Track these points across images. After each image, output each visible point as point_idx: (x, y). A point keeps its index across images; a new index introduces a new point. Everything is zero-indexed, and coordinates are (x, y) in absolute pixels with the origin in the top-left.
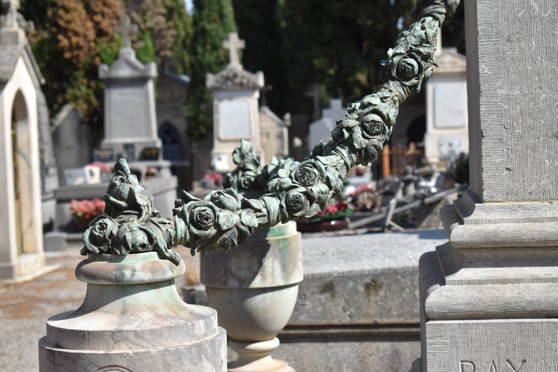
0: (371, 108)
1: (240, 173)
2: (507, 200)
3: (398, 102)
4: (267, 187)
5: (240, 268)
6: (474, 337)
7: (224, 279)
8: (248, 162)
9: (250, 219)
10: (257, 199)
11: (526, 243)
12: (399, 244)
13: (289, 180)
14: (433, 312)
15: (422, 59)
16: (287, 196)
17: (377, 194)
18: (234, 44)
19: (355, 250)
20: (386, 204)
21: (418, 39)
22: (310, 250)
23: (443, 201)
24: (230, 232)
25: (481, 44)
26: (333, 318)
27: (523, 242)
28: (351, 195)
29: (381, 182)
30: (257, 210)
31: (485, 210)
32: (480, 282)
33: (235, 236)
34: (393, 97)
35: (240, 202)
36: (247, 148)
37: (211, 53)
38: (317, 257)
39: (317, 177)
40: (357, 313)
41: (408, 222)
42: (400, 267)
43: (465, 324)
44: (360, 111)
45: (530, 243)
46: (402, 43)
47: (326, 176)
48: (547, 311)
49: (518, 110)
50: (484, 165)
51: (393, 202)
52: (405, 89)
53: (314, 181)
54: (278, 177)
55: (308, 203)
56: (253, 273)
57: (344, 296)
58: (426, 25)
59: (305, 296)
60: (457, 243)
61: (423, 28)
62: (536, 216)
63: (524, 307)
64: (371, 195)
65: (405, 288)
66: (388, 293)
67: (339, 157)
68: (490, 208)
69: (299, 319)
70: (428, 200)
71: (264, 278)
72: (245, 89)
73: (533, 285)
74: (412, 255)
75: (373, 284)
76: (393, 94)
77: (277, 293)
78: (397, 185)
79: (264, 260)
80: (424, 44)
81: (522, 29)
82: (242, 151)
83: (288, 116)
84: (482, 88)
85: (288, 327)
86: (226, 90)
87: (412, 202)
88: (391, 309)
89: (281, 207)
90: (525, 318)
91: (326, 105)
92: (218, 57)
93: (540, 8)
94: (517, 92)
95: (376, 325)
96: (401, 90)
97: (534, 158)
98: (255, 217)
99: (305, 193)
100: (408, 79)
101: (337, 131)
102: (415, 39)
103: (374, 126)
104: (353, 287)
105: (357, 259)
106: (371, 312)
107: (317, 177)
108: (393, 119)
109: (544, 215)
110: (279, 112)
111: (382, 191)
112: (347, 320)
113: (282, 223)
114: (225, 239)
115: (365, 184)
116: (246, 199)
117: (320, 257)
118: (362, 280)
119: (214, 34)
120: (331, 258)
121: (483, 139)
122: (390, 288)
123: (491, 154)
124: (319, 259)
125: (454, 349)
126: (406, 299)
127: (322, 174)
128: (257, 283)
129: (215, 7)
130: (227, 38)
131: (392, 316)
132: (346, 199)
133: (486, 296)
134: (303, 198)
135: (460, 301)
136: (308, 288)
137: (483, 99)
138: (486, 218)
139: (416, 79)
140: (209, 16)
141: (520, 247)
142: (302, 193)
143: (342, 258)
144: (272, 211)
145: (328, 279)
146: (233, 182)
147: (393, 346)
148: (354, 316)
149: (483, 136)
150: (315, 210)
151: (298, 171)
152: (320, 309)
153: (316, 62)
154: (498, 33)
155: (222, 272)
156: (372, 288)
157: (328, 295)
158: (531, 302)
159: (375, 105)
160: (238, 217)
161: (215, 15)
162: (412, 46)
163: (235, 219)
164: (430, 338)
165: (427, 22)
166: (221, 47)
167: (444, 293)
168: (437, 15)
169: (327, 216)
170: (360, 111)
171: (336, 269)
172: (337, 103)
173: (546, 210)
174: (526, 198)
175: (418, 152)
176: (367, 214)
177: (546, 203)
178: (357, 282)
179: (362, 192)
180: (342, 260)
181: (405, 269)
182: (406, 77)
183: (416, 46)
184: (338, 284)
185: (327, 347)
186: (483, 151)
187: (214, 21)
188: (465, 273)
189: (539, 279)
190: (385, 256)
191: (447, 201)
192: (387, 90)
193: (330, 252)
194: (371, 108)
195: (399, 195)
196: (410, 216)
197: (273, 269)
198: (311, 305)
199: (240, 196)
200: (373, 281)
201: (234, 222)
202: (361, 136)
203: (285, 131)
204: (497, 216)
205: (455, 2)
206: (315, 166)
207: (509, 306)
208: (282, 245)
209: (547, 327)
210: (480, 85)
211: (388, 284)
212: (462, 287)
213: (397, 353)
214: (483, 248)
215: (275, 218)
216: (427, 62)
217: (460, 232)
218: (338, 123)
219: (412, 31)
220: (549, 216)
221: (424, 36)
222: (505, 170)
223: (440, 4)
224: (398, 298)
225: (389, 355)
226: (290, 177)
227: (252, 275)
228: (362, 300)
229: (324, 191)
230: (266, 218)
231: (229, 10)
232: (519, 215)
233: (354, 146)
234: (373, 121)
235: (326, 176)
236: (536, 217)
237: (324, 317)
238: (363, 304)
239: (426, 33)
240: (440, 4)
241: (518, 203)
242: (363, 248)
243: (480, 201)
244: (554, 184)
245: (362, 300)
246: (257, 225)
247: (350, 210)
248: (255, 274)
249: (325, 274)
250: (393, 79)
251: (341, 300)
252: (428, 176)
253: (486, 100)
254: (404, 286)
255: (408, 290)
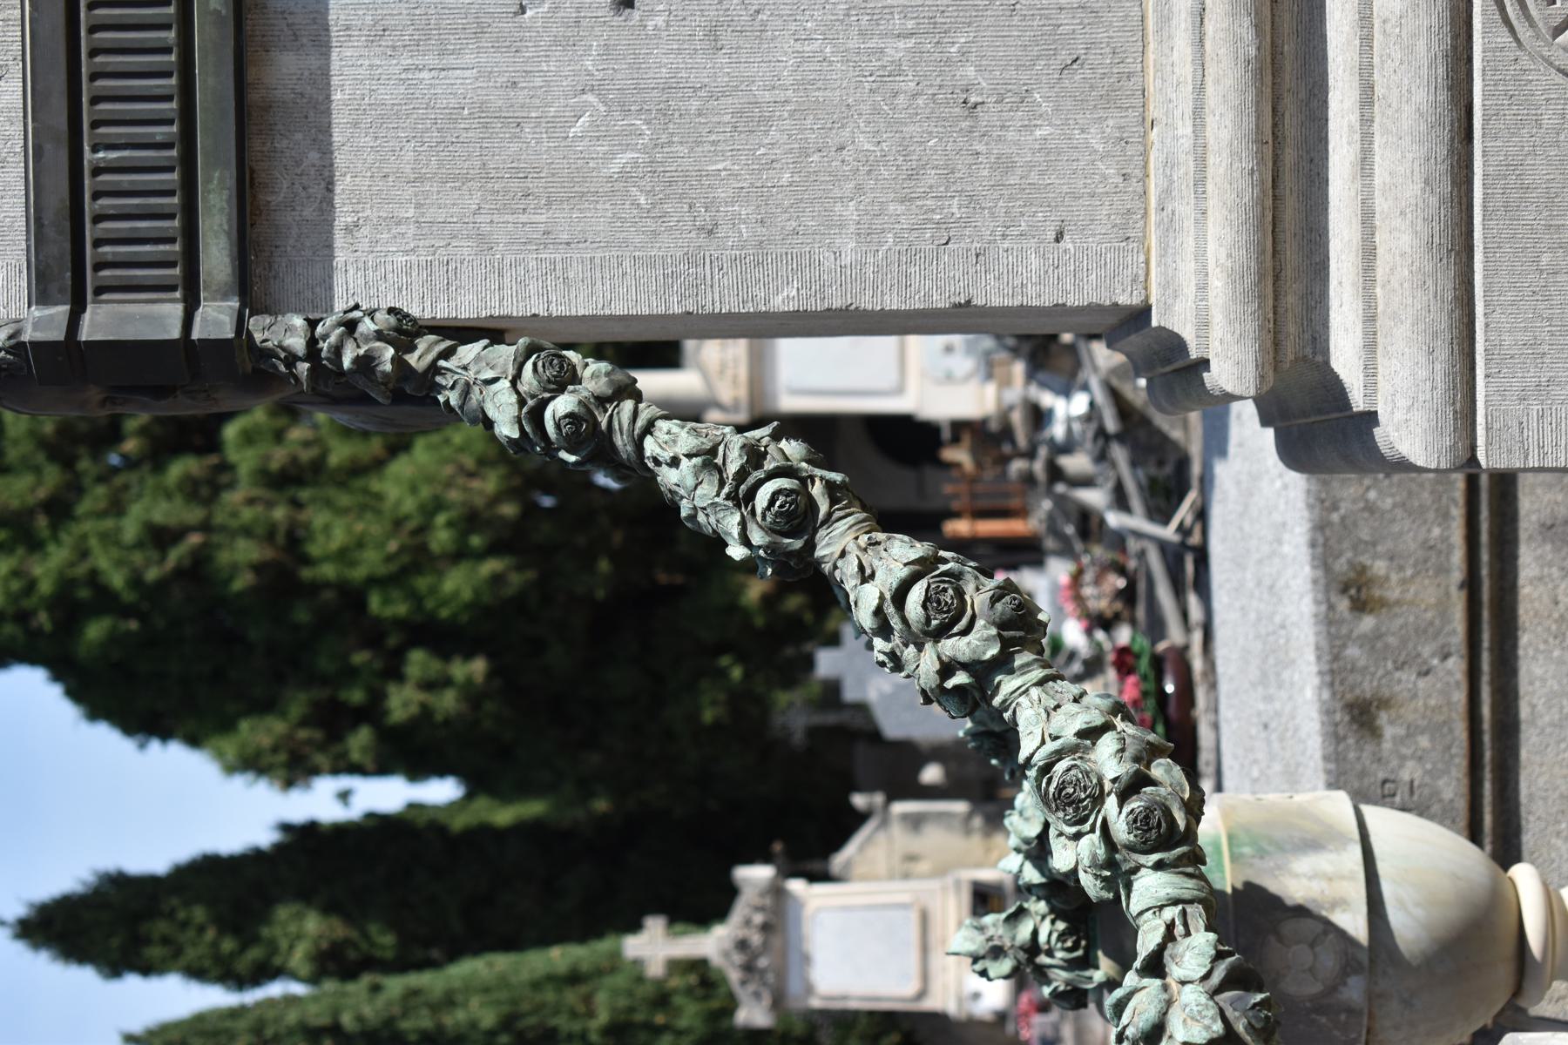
0: (890, 609)
1: (1043, 959)
2: (1143, 240)
3: (873, 535)
4: (1102, 903)
5: (1311, 970)
6: (1522, 337)
7: (1343, 1017)
8: (1013, 938)
9: (1195, 953)
10: (1136, 933)
11: (1263, 191)
12: (1242, 515)
13: (1085, 840)
14: (1453, 447)
15: (759, 466)
16: (1131, 848)
17: (1085, 560)
18: (653, 946)
19: (1258, 637)
20: (1118, 540)
21: (704, 476)
22: (1255, 761)
23: (1115, 382)
24: (1230, 1013)
25: (717, 304)
26: (1449, 703)
27: (1260, 202)
28: (1089, 632)
29: (1050, 543)
30: (1169, 936)
31: (1170, 301)
32: (1370, 319)
33: (1239, 998)
34: (859, 547)
35: (1146, 981)
36: (972, 940)
37: (678, 1012)
38: (1276, 745)
39: (1078, 762)
40: (1436, 636)
41: (1170, 481)
42: (1306, 514)
43: (1488, 361)
44: (897, 639)
45: (1262, 182)
46: (712, 520)
47: (1074, 740)
48: (1452, 139)
49: (901, 208)
50: (1047, 300)
51: (1114, 519)
52: (838, 514)
53: (1087, 773)
54: (1074, 871)
55: (1148, 789)
56: (1325, 933)
57: (1388, 673)
58: (666, 455)
59: (1385, 782)
60: (1262, 377)
61: (674, 462)
62: (1188, 166)
63: (1442, 201)
64: (1088, 577)
65: (1367, 501)
66: (1379, 548)
67: (1021, 699)
68: (1165, 286)
69: (1452, 801)
70: (1111, 425)
71: (1340, 903)
72: (778, 918)
73: (1380, 177)
74: (1272, 481)
75: (1353, 592)
76: (851, 547)
77: (1382, 867)
78: (1061, 501)
79: (1289, 902)
80: (719, 460)
81: (682, 197)
82: (982, 952)
83: (859, 800)
84: (837, 303)
85: (1475, 836)
86: (781, 973)
87: (1114, 465)
88: (1425, 541)
89: (1159, 866)
90: (1472, 198)
91: (833, 688)
92: (689, 991)
93: (628, 147)
94: (850, 211)
95: (1471, 584)
96: (841, 526)
97: (1030, 166)
98: (1188, 940)
99: (1123, 798)
100: (812, 505)
101: (952, 704)
102: (705, 485)
103: (939, 602)
104: (1361, 646)
105: (1283, 632)
106: (1432, 597)
107: (1078, 762)
108: (919, 550)
109: (1187, 143)
110: (847, 824)
111: (1078, 546)
112: (1456, 666)
113: (1204, 863)
114: (1250, 1027)
115: (1055, 589)
116: (1137, 964)
117: (1274, 737)
118: (1342, 621)
119: (623, 1002)
120: (1277, 705)
121: (974, 302)
122: (1366, 543)
123: (1018, 282)
124: (1282, 739)
125: (1556, 390)
126: (1398, 499)
127: (1072, 750)
128: (1354, 922)
129: (549, 996)
130: (638, 963)
131: (1444, 539)
132: (1099, 645)
133: (1410, 301)
134: (1134, 805)
135: (1423, 373)
136: (1363, 774)
137: (867, 302)
138: (1192, 297)
139: (813, 483)
140: (574, 1014)
141: (1275, 208)
142: (1121, 806)
143: (1278, 674)
144: (1173, 892)
145: (1338, 717)
146: (1067, 983)
147: (1530, 538)
148: (1443, 647)
149: (969, 302)
150: (1168, 771)
151: (1061, 814)
152: (1424, 742)
153: (708, 716)
154: (689, 259)
155: (1324, 1020)
156: (1363, 595)
157: (1383, 718)
158: (1427, 182)
159: (882, 598)
160: (1188, 987)
161: (571, 997)
162: (723, 495)
163: (1194, 996)
164: (1526, 457)
165: (658, 450)
166: (659, 983)
167: (1399, 416)
168: (640, 423)
169: (1151, 703)
170: (897, 639)
171: (1309, 693)
172: (827, 662)
173: (1172, 137)
174: (1140, 190)
175: (967, 439)
176: (1142, 587)
177: (1154, 135)
178: (1349, 636)
179: (1079, 599)
180: (1286, 675)
181: (1312, 501)
182: (805, 512)
183: (722, 484)
184: (1352, 689)
185: (1533, 723)
186: (1008, 302)
187: (588, 999)
188: (1345, 358)
189: (1364, 159)
190: (1273, 554)
191: (1115, 371)
192: (839, 563)
193: (1261, 706)
194: (890, 609)
195: (1094, 498)
196: (1153, 471)
197: (1314, 876)
198: (1410, 764)
199: (1131, 979)
200: (1344, 590)
201: (1203, 999)
202: (966, 639)
203: (900, 807)
204: (1187, 270)
205: (608, 374)
206: (1047, 769)
207: (1437, 240)
208: (1247, 850)
209: (1496, 138)
210: (829, 310)
211: (1355, 548)
212: (1384, 366)
213: (1552, 526)
214: (1275, 307)
215: (1191, 883)
216: (766, 453)
217: (1231, 365)
218: (928, 701)
219: (682, 492)
220: (1189, 130)
221: (696, 461)
222: (1062, 244)
223: (611, 416)
224: (1393, 521)
225: (1557, 550)
226: (1077, 837)
227: (1331, 936)
228: (1400, 621)
229: (1116, 746)
230: (1189, 909)
231: (559, 957)
232: (1185, 208)
233: (994, 659)
234: (924, 606)
235: (1074, 740)
236: (1191, 164)
237: (1445, 730)
238: (1411, 619)
239: (689, 456)
240: (611, 416)
241: (1152, 212)
242: (1253, 616)
243: (1144, 312)
244: (1101, 113)
245: (1400, 621)
246: (1212, 936)
247: (1133, 639)
248: (1328, 924)
249: (1323, 723)
250: (811, 546)
251: (1399, 681)
252: (1039, 417)
253: (869, 293)
254: (1362, 505)
255: (1372, 495)
